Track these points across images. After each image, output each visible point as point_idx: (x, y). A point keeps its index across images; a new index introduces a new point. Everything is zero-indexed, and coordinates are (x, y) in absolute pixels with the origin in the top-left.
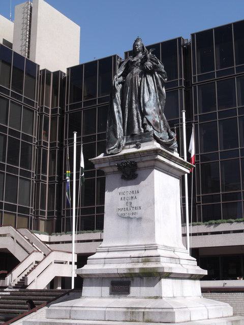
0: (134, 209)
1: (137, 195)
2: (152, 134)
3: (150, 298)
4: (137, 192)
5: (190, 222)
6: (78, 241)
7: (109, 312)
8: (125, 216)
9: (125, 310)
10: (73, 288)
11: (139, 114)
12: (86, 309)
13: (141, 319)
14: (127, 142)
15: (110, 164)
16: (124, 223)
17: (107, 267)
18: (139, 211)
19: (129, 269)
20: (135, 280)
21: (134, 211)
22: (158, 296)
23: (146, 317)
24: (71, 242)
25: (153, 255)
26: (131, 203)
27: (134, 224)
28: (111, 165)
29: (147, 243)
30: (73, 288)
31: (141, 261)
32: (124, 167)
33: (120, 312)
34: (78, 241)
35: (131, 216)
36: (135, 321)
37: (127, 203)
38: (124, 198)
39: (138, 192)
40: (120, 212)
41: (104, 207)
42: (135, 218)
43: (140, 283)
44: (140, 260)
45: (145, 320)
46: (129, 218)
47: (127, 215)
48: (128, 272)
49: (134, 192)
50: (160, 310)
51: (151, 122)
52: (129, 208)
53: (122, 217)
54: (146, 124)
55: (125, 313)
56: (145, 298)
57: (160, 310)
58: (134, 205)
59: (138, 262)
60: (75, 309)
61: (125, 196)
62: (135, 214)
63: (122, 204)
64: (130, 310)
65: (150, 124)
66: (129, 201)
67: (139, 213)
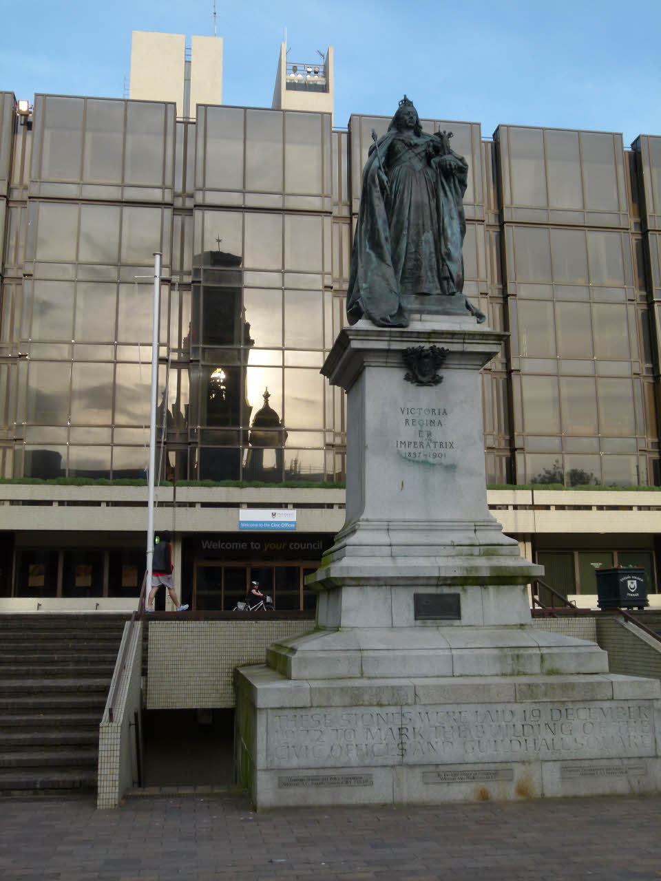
0: (438, 445)
1: (442, 418)
4: (442, 411)
6: (161, 504)
7: (461, 657)
8: (417, 459)
9: (496, 652)
10: (302, 609)
11: (434, 255)
13: (536, 668)
15: (389, 345)
16: (413, 475)
17: (401, 562)
18: (450, 452)
23: (547, 665)
24: (145, 504)
25: (363, 543)
26: (429, 434)
27: (437, 478)
30: (302, 609)
32: (427, 356)
34: (161, 504)
35: (431, 460)
37: (420, 431)
38: (414, 421)
39: (445, 412)
40: (405, 450)
42: (440, 464)
44: (476, 550)
46: (425, 463)
47: (422, 458)
48: (465, 574)
49: (437, 411)
52: (425, 443)
53: (410, 460)
54: (446, 278)
57: (573, 650)
58: (437, 435)
59: (472, 555)
62: (440, 456)
63: (408, 433)
65: (453, 281)
66: (425, 428)
67: (451, 456)
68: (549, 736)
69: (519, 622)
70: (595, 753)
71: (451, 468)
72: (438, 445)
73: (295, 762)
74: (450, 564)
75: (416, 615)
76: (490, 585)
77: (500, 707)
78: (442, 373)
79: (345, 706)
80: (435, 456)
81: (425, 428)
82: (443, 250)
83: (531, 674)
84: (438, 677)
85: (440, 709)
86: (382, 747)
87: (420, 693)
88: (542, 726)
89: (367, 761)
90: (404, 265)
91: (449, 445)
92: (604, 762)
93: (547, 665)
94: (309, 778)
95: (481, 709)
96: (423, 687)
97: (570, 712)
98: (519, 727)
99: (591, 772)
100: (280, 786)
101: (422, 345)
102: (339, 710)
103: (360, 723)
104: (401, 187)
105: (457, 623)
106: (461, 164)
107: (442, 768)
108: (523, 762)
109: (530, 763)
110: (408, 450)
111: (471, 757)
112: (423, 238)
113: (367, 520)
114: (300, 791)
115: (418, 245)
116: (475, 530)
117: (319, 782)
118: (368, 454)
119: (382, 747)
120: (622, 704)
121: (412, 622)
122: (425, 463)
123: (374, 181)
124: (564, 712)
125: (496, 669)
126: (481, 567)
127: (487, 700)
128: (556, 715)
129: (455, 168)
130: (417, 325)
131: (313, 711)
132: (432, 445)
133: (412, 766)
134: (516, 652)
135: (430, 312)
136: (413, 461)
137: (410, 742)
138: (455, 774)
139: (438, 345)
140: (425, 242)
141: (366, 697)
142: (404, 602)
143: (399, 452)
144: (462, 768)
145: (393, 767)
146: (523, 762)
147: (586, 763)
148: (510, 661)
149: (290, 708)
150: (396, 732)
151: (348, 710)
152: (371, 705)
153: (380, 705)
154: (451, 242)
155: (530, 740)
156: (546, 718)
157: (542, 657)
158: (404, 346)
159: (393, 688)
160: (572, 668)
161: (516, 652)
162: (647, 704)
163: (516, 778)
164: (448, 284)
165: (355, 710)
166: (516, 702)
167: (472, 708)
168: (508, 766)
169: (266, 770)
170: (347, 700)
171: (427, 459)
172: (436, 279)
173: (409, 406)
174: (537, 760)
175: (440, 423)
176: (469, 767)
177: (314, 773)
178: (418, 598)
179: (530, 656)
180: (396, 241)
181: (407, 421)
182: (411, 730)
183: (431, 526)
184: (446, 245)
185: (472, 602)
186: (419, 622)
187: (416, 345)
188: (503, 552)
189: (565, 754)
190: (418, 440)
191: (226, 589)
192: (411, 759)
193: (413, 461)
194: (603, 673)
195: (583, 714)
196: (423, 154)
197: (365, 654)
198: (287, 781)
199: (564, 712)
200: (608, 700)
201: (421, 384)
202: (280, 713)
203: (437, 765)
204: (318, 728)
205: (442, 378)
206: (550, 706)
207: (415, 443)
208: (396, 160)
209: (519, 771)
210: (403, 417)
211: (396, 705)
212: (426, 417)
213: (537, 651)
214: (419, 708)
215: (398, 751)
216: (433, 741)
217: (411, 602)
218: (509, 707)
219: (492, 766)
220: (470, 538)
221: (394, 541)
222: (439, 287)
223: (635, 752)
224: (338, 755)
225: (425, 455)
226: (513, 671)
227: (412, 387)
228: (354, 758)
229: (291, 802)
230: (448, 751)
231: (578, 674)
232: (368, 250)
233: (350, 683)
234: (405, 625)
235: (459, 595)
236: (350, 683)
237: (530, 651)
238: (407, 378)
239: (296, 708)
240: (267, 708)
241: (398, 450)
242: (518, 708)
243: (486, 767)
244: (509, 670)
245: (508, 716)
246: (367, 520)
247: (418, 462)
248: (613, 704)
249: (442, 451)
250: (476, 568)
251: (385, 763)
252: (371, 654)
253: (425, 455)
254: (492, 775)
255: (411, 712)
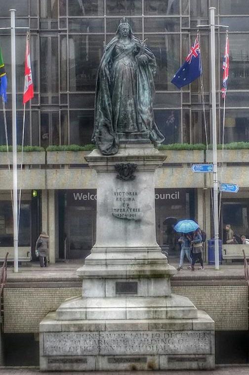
0: (132, 210)
1: (134, 197)
2: (159, 143)
3: (158, 297)
5: (19, 142)
7: (130, 311)
9: (146, 309)
11: (134, 111)
12: (73, 310)
13: (164, 316)
14: (121, 140)
16: (120, 225)
17: (110, 269)
18: (138, 214)
19: (140, 271)
20: (142, 281)
21: (133, 213)
22: (167, 295)
26: (128, 205)
27: (131, 226)
28: (108, 164)
29: (148, 246)
31: (147, 263)
32: (126, 168)
33: (142, 311)
35: (128, 217)
36: (158, 319)
37: (124, 204)
39: (136, 194)
41: (214, 247)
42: (133, 220)
43: (148, 284)
45: (168, 317)
47: (124, 217)
50: (182, 309)
51: (146, 121)
52: (126, 210)
55: (148, 312)
56: (154, 297)
57: (182, 309)
60: (90, 310)
61: (122, 197)
63: (117, 205)
64: (152, 309)
66: (126, 202)
68: (163, 345)
69: (164, 295)
70: (184, 352)
71: (138, 221)
72: (132, 210)
73: (55, 353)
74: (132, 269)
75: (116, 292)
76: (152, 278)
77: (142, 333)
78: (135, 174)
79: (76, 332)
80: (131, 215)
81: (126, 202)
82: (139, 107)
83: (162, 319)
84: (72, 320)
85: (115, 333)
86: (91, 348)
87: (107, 326)
88: (160, 340)
89: (85, 353)
90: (119, 116)
91: (137, 210)
92: (187, 356)
93: (169, 315)
94: (61, 360)
95: (134, 333)
96: (109, 324)
97: (173, 335)
98: (150, 340)
99: (182, 360)
100: (49, 363)
101: (123, 162)
102: (73, 333)
103: (82, 338)
104: (117, 75)
105: (135, 295)
106: (150, 58)
107: (116, 357)
108: (151, 355)
109: (154, 355)
110: (117, 213)
111: (128, 352)
112: (128, 103)
113: (97, 248)
114: (57, 364)
115: (126, 106)
116: (148, 252)
117: (64, 361)
118: (98, 215)
119: (91, 348)
120: (197, 332)
121: (115, 295)
122: (126, 219)
123: (102, 74)
124: (170, 335)
125: (146, 316)
126: (146, 270)
127: (136, 330)
128: (167, 336)
129: (146, 62)
130: (123, 153)
131: (63, 333)
132: (129, 210)
133: (104, 356)
134: (155, 309)
135: (131, 143)
136: (120, 219)
137: (103, 346)
138: (122, 359)
139: (131, 162)
140: (130, 105)
141: (85, 328)
142: (110, 287)
143: (113, 214)
144: (124, 357)
145: (95, 356)
146: (151, 355)
147: (179, 356)
148: (152, 313)
149: (53, 332)
150: (97, 342)
151: (77, 333)
152: (86, 331)
153: (90, 331)
154: (142, 104)
155: (155, 346)
156: (162, 336)
157: (167, 312)
158: (115, 163)
159: (96, 324)
160: (181, 316)
161: (155, 309)
162: (208, 332)
163: (148, 362)
164: (141, 126)
165: (81, 333)
166: (149, 330)
167: (129, 333)
168: (145, 356)
169: (44, 356)
170: (77, 329)
171: (127, 217)
172: (135, 124)
173: (119, 191)
174: (157, 354)
175: (133, 199)
176: (127, 357)
177: (63, 357)
178: (117, 284)
179: (161, 311)
180: (114, 104)
181: (117, 199)
182: (103, 341)
183: (127, 251)
184: (140, 106)
185: (142, 288)
186: (117, 295)
187: (120, 163)
188: (160, 263)
189: (170, 352)
190: (123, 208)
191: (67, 111)
192: (102, 352)
193: (120, 219)
194: (83, 320)
195: (179, 336)
196: (131, 53)
197: (88, 310)
198: (51, 360)
199: (170, 335)
200: (191, 330)
201: (125, 180)
202: (49, 334)
203: (114, 356)
204: (65, 340)
205: (135, 177)
206: (164, 333)
207: (121, 209)
208: (117, 58)
209: (149, 358)
210: (115, 197)
211: (97, 331)
212: (126, 197)
213: (165, 309)
214: (107, 333)
215: (98, 349)
216: (113, 345)
217: (114, 286)
218: (145, 333)
219: (138, 356)
220: (145, 256)
221: (107, 258)
222: (136, 128)
223: (201, 351)
224: (73, 350)
225: (126, 215)
226: (153, 317)
227: (120, 182)
228: (79, 352)
229: (54, 369)
230: (119, 350)
231: (183, 319)
232: (100, 110)
233: (78, 322)
234: (111, 296)
235: (137, 283)
236: (78, 322)
237: (162, 309)
238: (118, 178)
239: (55, 332)
240: (43, 332)
241: (113, 214)
242: (150, 333)
243: (135, 357)
244: (151, 316)
245: (145, 336)
246: (97, 248)
247: (122, 219)
248: (192, 332)
249: (134, 213)
250: (144, 271)
251: (92, 354)
252: (90, 310)
253: (126, 215)
254: (138, 360)
255: (104, 334)
